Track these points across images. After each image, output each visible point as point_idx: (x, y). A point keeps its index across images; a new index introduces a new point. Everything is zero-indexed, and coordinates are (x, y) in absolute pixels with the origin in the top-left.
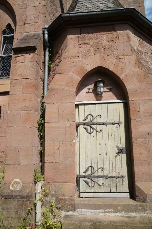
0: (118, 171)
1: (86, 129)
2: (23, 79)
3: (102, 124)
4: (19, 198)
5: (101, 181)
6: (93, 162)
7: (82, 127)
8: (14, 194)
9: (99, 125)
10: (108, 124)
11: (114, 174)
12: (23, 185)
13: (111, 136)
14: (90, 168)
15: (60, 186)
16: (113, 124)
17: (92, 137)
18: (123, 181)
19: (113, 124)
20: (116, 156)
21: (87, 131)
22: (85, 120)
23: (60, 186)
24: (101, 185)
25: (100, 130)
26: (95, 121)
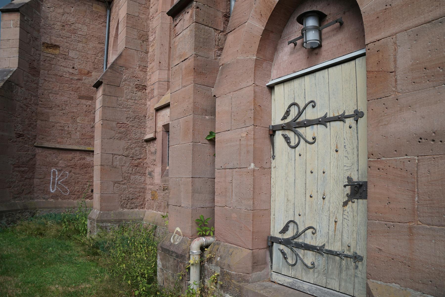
0: (346, 240)
1: (271, 135)
2: (182, 61)
3: (317, 124)
4: (174, 255)
5: (309, 257)
6: (297, 214)
7: (279, 134)
8: (172, 249)
9: (310, 127)
10: (330, 122)
11: (336, 247)
12: (183, 238)
13: (337, 151)
14: (291, 226)
15: (231, 250)
16: (341, 118)
17: (297, 155)
18: (357, 267)
19: (341, 118)
20: (345, 204)
21: (289, 143)
22: (284, 118)
23: (231, 250)
24: (309, 265)
25: (313, 139)
26: (302, 118)
